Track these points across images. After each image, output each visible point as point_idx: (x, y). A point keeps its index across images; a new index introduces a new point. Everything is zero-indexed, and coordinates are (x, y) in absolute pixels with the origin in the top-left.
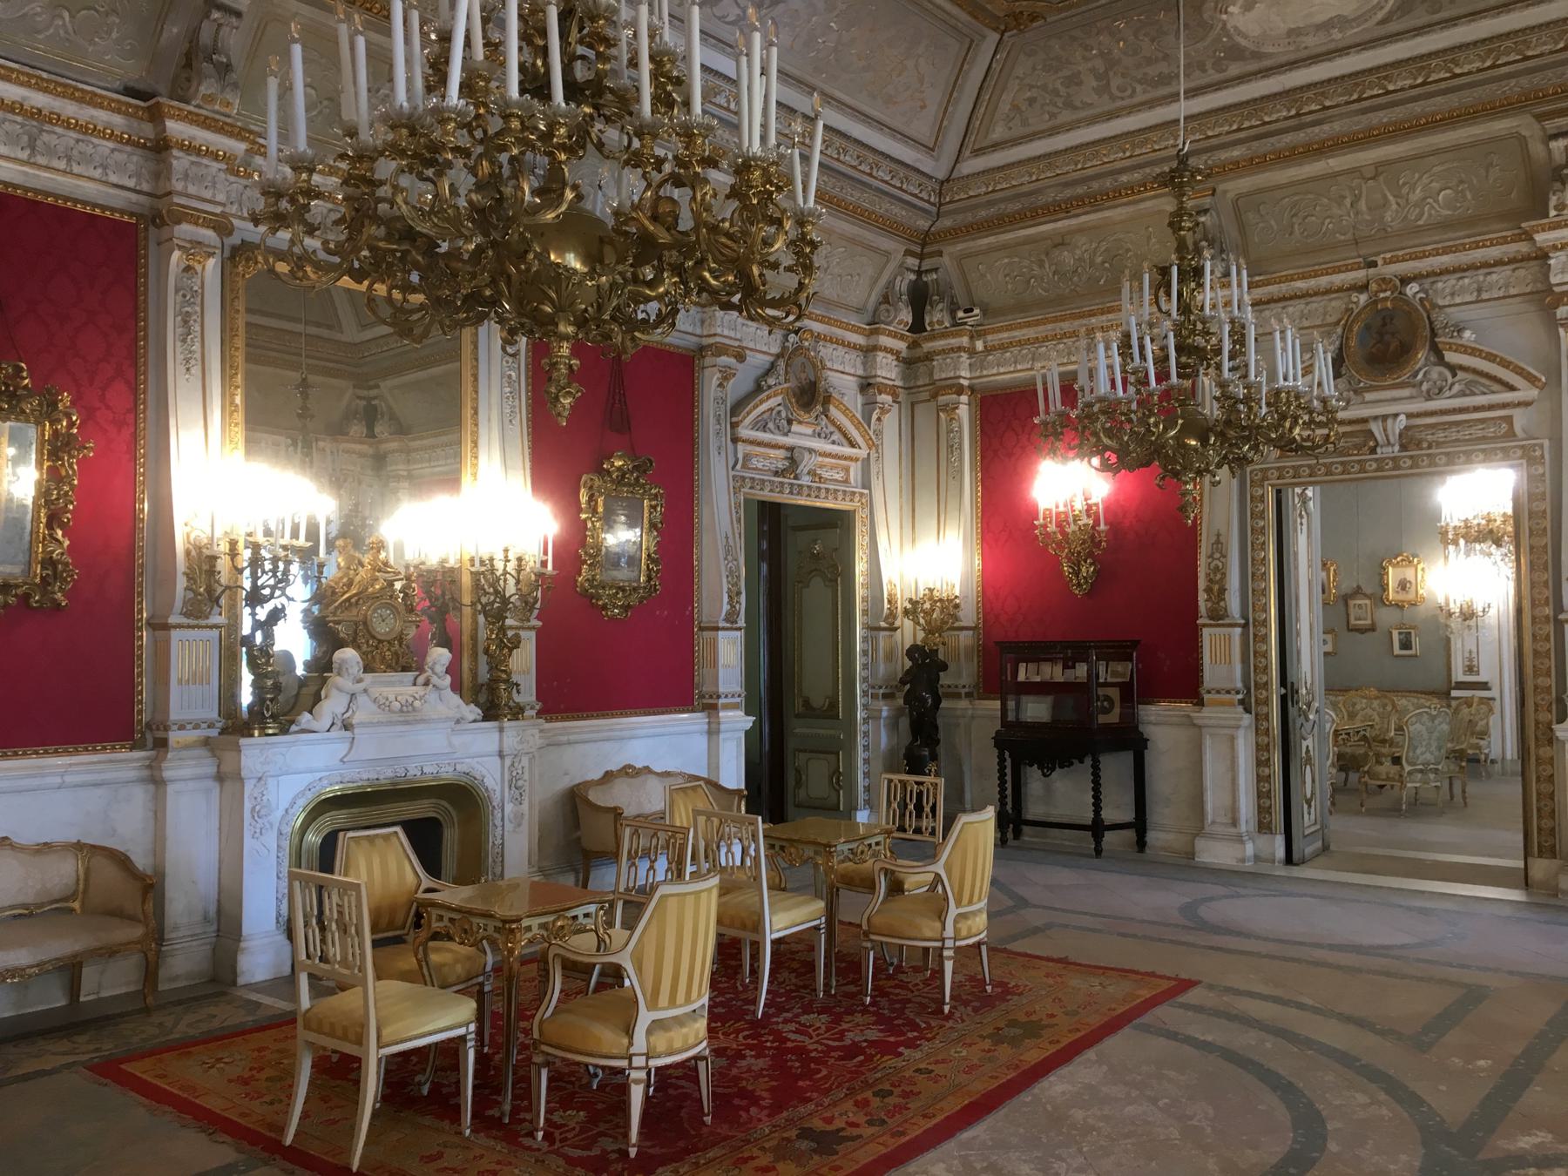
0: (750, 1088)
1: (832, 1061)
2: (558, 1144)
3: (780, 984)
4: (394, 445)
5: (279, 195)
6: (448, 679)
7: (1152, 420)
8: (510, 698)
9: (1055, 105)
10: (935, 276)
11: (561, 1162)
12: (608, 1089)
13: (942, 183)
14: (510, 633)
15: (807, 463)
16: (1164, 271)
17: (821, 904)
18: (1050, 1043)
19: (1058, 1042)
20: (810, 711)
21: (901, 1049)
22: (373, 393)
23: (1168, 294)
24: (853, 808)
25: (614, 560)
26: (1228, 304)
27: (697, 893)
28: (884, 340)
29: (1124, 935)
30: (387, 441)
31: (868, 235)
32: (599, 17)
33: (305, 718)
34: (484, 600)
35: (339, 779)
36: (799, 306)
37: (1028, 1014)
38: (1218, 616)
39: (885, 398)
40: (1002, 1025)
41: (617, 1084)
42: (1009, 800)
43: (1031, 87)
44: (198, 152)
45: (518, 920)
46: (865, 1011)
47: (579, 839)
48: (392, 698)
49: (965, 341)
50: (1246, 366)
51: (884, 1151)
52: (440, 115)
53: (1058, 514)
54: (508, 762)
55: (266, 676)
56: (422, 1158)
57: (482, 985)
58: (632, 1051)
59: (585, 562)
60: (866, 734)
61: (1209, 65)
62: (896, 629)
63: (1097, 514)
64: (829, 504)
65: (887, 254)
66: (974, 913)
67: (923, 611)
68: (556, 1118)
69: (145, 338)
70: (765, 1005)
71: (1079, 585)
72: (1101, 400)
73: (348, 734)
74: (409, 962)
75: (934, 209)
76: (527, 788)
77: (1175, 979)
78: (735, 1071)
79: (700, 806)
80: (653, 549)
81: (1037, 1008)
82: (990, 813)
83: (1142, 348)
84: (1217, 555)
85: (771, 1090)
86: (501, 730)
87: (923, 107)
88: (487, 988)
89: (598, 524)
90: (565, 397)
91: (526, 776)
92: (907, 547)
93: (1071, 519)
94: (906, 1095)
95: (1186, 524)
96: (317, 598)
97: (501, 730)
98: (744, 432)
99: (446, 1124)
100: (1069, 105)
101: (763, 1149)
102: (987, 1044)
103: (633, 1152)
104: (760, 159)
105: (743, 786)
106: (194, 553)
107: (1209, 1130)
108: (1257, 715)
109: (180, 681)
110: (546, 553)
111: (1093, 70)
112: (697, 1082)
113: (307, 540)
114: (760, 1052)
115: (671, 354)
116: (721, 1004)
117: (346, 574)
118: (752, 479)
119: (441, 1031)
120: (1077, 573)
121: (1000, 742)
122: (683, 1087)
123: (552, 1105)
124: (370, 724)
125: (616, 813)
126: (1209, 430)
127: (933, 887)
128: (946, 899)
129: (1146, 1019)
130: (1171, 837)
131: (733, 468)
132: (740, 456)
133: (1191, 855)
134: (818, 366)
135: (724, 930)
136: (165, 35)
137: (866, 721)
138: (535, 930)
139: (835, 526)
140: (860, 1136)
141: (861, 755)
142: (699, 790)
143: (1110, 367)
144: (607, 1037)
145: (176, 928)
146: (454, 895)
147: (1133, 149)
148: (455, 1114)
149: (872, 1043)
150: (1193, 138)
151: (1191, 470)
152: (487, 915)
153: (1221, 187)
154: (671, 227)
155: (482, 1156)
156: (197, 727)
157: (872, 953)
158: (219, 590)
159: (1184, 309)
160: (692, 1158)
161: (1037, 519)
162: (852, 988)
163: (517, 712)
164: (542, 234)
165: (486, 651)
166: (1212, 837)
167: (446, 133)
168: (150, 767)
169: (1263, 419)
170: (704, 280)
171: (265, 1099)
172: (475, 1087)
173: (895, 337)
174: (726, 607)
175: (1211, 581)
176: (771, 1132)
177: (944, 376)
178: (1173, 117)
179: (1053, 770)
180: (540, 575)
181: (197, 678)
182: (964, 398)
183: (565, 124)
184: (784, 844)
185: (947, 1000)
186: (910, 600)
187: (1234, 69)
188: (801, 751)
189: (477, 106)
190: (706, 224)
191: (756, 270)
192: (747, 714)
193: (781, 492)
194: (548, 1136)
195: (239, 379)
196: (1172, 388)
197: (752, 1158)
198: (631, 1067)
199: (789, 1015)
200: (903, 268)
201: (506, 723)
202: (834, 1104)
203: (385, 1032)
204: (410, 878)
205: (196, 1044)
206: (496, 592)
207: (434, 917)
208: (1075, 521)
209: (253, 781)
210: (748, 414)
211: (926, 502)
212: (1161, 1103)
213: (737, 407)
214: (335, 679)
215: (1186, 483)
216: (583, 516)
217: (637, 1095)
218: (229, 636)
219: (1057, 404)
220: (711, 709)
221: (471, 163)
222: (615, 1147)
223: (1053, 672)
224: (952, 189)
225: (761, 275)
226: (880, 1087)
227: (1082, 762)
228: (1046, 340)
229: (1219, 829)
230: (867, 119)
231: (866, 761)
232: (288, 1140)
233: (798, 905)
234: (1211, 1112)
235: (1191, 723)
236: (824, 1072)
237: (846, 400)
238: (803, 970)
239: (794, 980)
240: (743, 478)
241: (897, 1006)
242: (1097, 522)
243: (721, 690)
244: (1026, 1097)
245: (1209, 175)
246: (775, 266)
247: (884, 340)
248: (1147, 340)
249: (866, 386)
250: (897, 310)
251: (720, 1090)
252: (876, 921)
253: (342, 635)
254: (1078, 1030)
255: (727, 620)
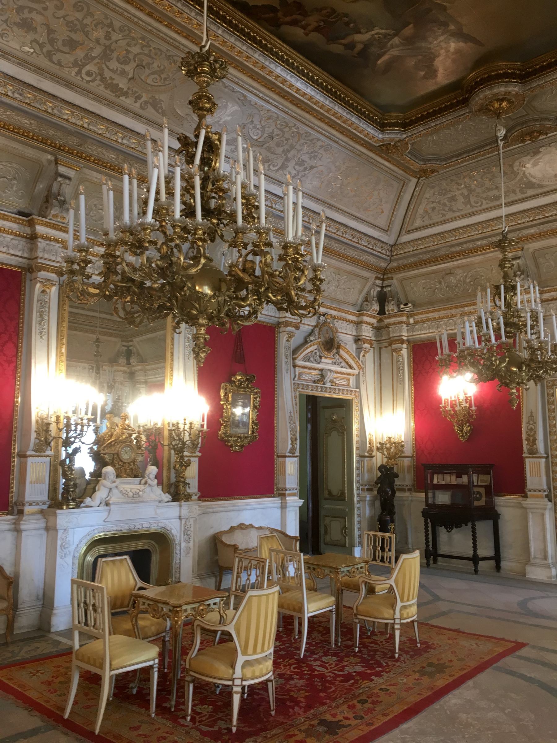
0: (295, 696)
1: (337, 682)
2: (197, 724)
3: (313, 639)
4: (139, 368)
5: (72, 263)
6: (156, 481)
7: (493, 358)
8: (185, 491)
9: (444, 210)
10: (389, 289)
11: (199, 734)
12: (224, 694)
13: (392, 246)
14: (186, 459)
15: (329, 377)
16: (498, 287)
17: (333, 599)
18: (450, 676)
19: (453, 675)
20: (331, 497)
21: (373, 677)
22: (130, 344)
23: (500, 298)
24: (352, 546)
25: (236, 424)
26: (529, 302)
27: (268, 595)
28: (366, 319)
29: (489, 617)
30: (136, 366)
31: (357, 270)
32: (220, 180)
33: (88, 500)
34: (174, 443)
35: (102, 530)
36: (315, 309)
37: (438, 660)
38: (533, 452)
39: (367, 346)
40: (425, 665)
41: (227, 692)
42: (431, 544)
43: (433, 202)
44: (50, 239)
45: (180, 606)
46: (355, 656)
47: (217, 560)
48: (129, 490)
49: (404, 319)
50: (539, 332)
51: (361, 733)
52: (143, 226)
53: (451, 401)
54: (183, 522)
55: (70, 480)
56: (130, 728)
57: (164, 637)
58: (235, 676)
59: (222, 425)
60: (359, 509)
61: (518, 190)
62: (373, 457)
63: (471, 401)
64: (340, 396)
65: (366, 279)
66: (410, 606)
67: (386, 448)
68: (197, 709)
69: (23, 323)
70: (305, 651)
71: (463, 436)
72: (468, 349)
73: (107, 508)
74: (128, 626)
75: (389, 258)
76: (192, 535)
77: (513, 642)
78: (288, 687)
79: (275, 547)
80: (255, 418)
81: (443, 656)
82: (417, 553)
83: (487, 323)
84: (531, 422)
85: (306, 697)
86: (180, 506)
87: (382, 212)
88: (167, 639)
89: (229, 407)
90: (202, 353)
91: (192, 529)
92: (378, 415)
93: (458, 404)
94: (374, 703)
95: (513, 409)
96: (97, 442)
97: (180, 506)
98: (299, 362)
99: (143, 710)
100: (451, 210)
101: (300, 730)
102: (417, 676)
103: (234, 730)
104: (292, 243)
105: (298, 535)
106: (40, 422)
107: (532, 727)
108: (555, 503)
109: (31, 483)
110: (203, 420)
111: (462, 194)
112: (267, 691)
113: (92, 415)
114: (301, 676)
115: (264, 326)
116: (281, 650)
117: (110, 431)
118: (303, 384)
119: (136, 664)
120: (462, 431)
121: (425, 514)
122: (261, 694)
123: (196, 702)
124: (118, 503)
125: (235, 548)
126: (522, 363)
127: (389, 592)
128: (396, 598)
129: (499, 664)
130: (514, 564)
131: (294, 379)
132: (297, 374)
133: (524, 574)
134: (334, 331)
135: (283, 611)
136: (37, 188)
137: (359, 502)
138: (189, 611)
139: (343, 407)
140: (350, 725)
141: (356, 519)
142: (125, 562)
143: (472, 332)
144: (222, 669)
145: (23, 603)
146: (152, 592)
147: (483, 230)
148: (146, 704)
149: (358, 673)
150: (511, 224)
151: (514, 383)
152: (166, 603)
153: (526, 247)
154: (252, 274)
155: (159, 729)
156: (37, 504)
157: (358, 625)
158: (51, 439)
159: (508, 305)
160: (263, 734)
161: (441, 404)
162: (349, 643)
163: (188, 498)
164: (193, 278)
165: (174, 468)
166: (534, 565)
167: (146, 234)
168: (14, 523)
169: (550, 358)
170: (269, 297)
171: (58, 693)
172: (158, 691)
173: (371, 317)
174: (290, 446)
175: (529, 435)
176: (305, 721)
177: (395, 335)
178: (499, 215)
179: (452, 529)
180: (200, 431)
181: (38, 481)
182: (405, 346)
183: (202, 229)
184: (315, 567)
185: (397, 651)
186: (380, 443)
187: (530, 192)
188: (326, 516)
189: (160, 221)
190: (267, 272)
191: (293, 293)
192: (300, 498)
193: (317, 391)
194: (193, 719)
195: (64, 341)
196: (503, 343)
197: (295, 735)
198: (234, 685)
199: (316, 656)
200: (374, 284)
201: (183, 503)
202: (337, 707)
203: (114, 663)
204: (132, 581)
205: (27, 663)
206: (180, 439)
207: (141, 603)
208: (460, 405)
209: (62, 531)
210: (301, 354)
211: (387, 395)
212: (506, 711)
213: (295, 351)
214: (103, 482)
215: (512, 389)
216: (222, 403)
217: (236, 699)
218: (55, 460)
219: (446, 350)
220: (282, 495)
221: (158, 247)
222: (226, 726)
223: (451, 479)
224: (396, 249)
225: (297, 295)
226: (361, 698)
227: (466, 525)
228: (444, 318)
229: (538, 561)
230: (356, 218)
231: (359, 522)
232: (66, 716)
233: (320, 599)
234: (533, 717)
235: (520, 506)
236: (333, 689)
237: (347, 347)
238: (324, 632)
239: (320, 638)
240: (298, 384)
241: (371, 653)
242: (471, 406)
243: (288, 486)
244: (436, 706)
245: (518, 242)
246: (303, 290)
247: (366, 319)
248: (490, 320)
249: (358, 340)
250: (372, 305)
251: (280, 697)
252: (361, 608)
253: (107, 460)
254: (464, 669)
255: (290, 452)
